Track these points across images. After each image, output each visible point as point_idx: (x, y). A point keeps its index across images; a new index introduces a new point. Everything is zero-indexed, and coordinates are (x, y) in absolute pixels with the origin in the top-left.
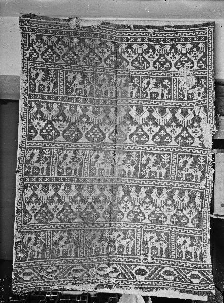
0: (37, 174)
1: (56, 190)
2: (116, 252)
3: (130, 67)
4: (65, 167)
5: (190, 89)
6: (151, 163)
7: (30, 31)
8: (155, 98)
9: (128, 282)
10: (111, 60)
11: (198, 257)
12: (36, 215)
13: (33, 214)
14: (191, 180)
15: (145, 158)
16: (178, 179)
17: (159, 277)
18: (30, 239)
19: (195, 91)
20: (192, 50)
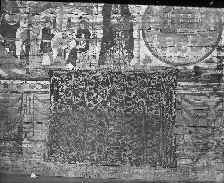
2: (158, 115)
3: (69, 108)
4: (116, 141)
6: (115, 98)
8: (84, 97)
12: (138, 155)
19: (81, 79)
20: (62, 99)
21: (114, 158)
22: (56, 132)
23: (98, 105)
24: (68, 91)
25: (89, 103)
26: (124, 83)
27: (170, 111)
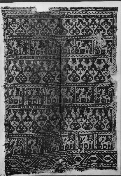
0: (16, 103)
1: (28, 113)
3: (68, 34)
4: (33, 99)
5: (103, 47)
6: (82, 93)
7: (9, 17)
8: (83, 53)
9: (71, 165)
10: (57, 30)
11: (110, 147)
12: (17, 128)
13: (15, 128)
14: (105, 102)
15: (78, 90)
16: (98, 102)
17: (88, 161)
18: (14, 142)
19: (105, 48)
21: (13, 96)
22: (38, 22)
23: (74, 71)
24: (88, 31)
25: (77, 60)
26: (100, 103)
27: (69, 163)
